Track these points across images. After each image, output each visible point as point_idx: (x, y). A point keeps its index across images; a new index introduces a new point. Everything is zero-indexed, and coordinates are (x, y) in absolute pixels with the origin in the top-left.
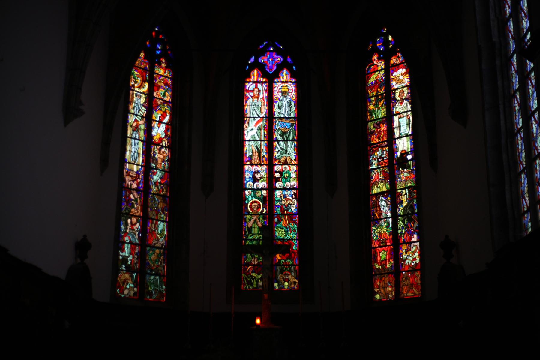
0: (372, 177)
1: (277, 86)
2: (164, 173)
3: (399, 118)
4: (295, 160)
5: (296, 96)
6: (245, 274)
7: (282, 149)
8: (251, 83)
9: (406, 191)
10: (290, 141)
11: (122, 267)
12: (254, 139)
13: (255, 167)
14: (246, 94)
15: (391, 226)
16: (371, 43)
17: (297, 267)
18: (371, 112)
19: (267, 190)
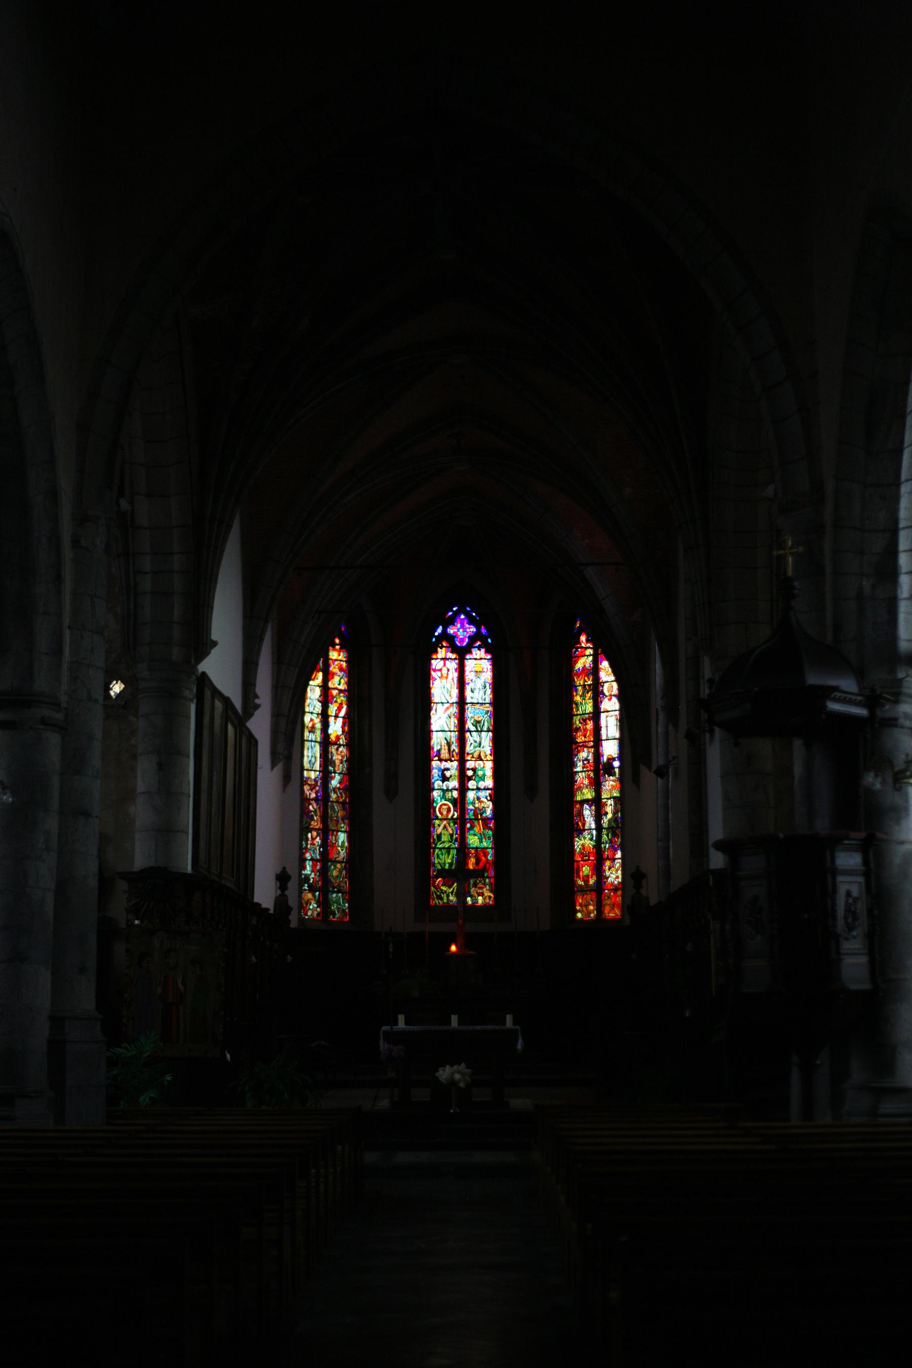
2: (342, 775)
3: (607, 717)
4: (491, 755)
7: (475, 742)
12: (443, 729)
13: (444, 763)
15: (594, 838)
16: (579, 620)
17: (492, 880)
18: (577, 704)
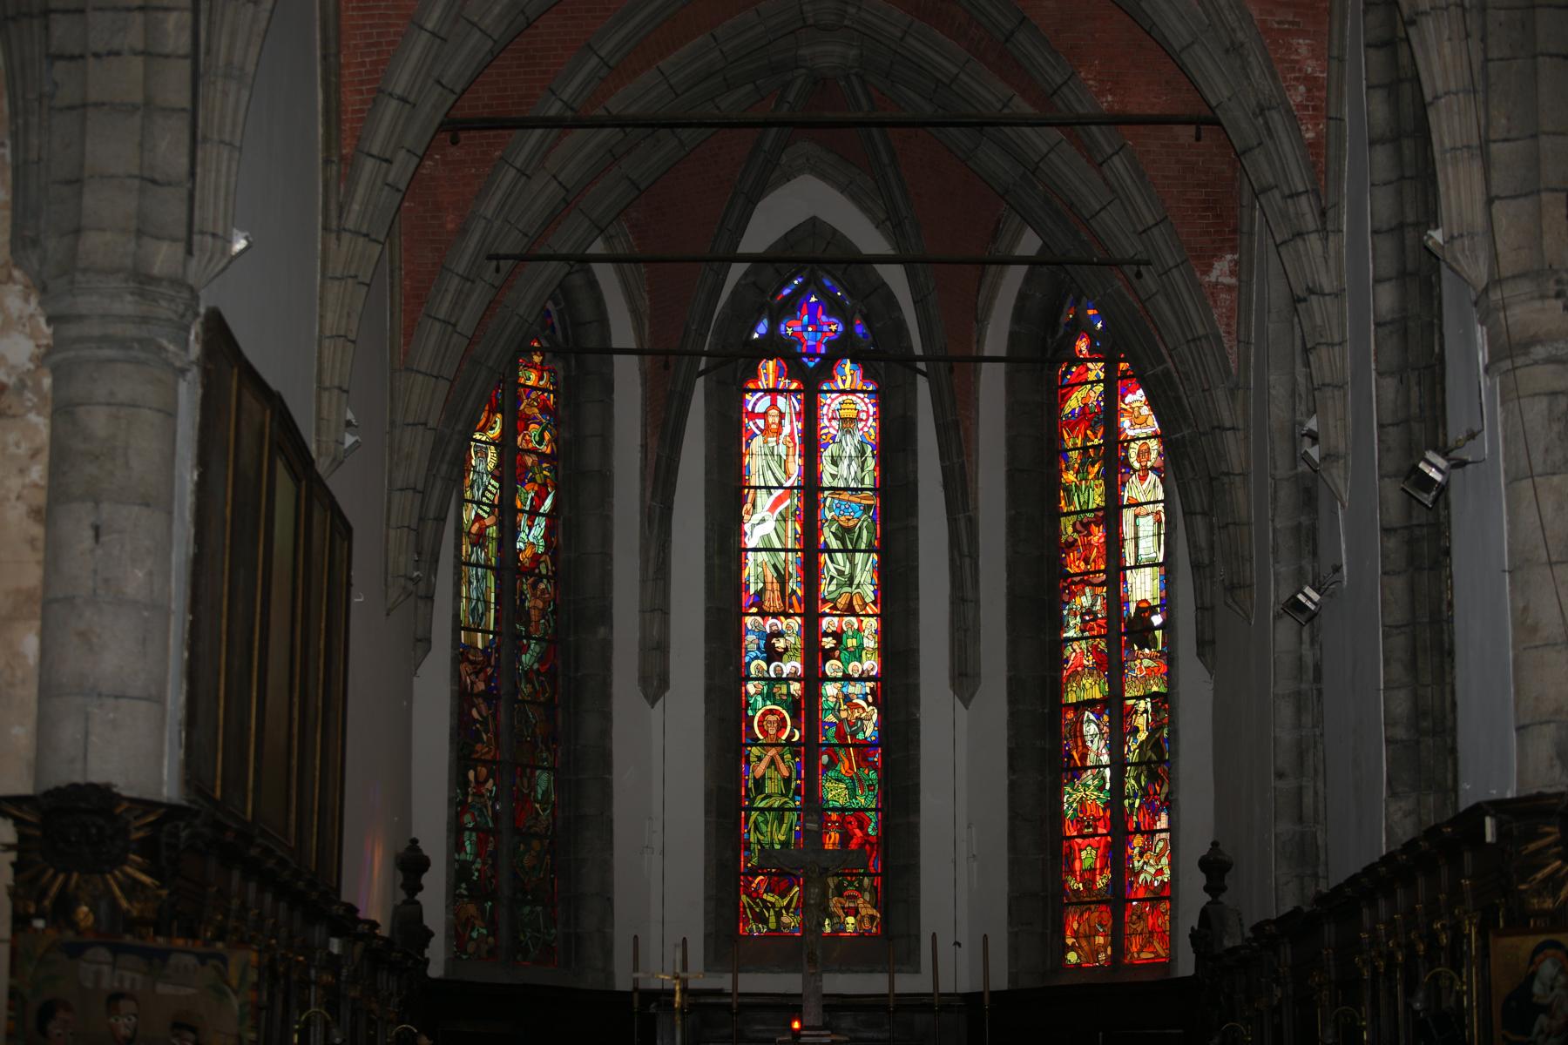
0: (1067, 661)
1: (829, 401)
3: (1136, 516)
5: (878, 431)
6: (749, 895)
7: (841, 573)
8: (760, 394)
9: (1146, 703)
10: (860, 551)
11: (461, 888)
12: (769, 547)
13: (771, 621)
14: (747, 422)
15: (1108, 786)
17: (878, 880)
18: (1068, 490)
19: (803, 682)
